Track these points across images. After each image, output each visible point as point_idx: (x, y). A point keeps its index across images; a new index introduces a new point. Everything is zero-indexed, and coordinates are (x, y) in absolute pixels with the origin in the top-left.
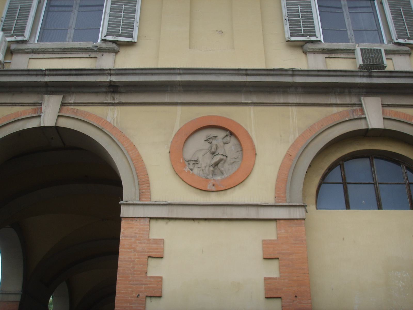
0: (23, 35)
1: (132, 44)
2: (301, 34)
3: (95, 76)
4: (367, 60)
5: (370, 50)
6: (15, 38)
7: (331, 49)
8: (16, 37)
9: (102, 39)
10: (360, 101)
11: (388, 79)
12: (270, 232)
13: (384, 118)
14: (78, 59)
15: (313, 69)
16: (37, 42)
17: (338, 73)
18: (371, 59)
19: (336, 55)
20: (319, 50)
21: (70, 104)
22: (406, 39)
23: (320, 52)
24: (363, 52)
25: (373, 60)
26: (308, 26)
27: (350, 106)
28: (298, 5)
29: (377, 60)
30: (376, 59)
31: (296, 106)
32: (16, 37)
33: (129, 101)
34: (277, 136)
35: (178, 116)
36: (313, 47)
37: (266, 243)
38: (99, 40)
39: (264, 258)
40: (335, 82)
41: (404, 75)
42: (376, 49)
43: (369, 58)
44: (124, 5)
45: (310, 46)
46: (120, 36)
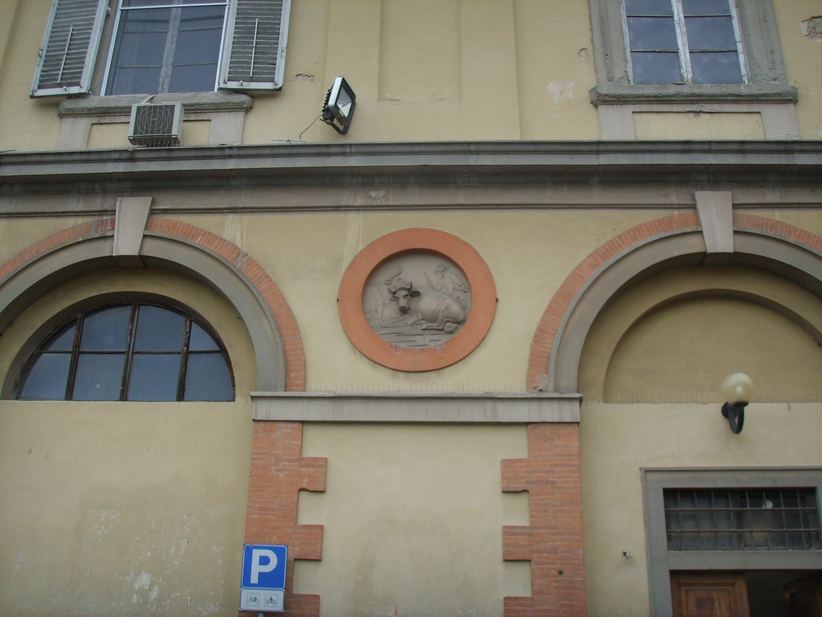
0: (78, 84)
1: (274, 94)
2: (248, 76)
3: (511, 156)
4: (142, 128)
5: (154, 109)
6: (66, 90)
7: (102, 108)
8: (243, 83)
9: (220, 88)
10: (694, 198)
11: (315, 159)
12: (515, 445)
13: (735, 232)
14: (654, 115)
15: (312, 142)
16: (105, 95)
17: (76, 157)
18: (151, 125)
19: (112, 118)
20: (83, 111)
21: (166, 211)
22: (241, 81)
23: (85, 114)
24: (140, 112)
25: (153, 128)
26: (75, 66)
27: (98, 215)
28: (255, 19)
29: (161, 127)
30: (159, 125)
31: (6, 217)
32: (67, 89)
33: (504, 202)
34: (534, 266)
35: (352, 232)
36: (73, 106)
37: (507, 465)
38: (216, 90)
39: (505, 492)
40: (68, 173)
41: (193, 154)
42: (165, 106)
43: (141, 123)
44: (257, 19)
45: (68, 105)
46: (251, 80)
